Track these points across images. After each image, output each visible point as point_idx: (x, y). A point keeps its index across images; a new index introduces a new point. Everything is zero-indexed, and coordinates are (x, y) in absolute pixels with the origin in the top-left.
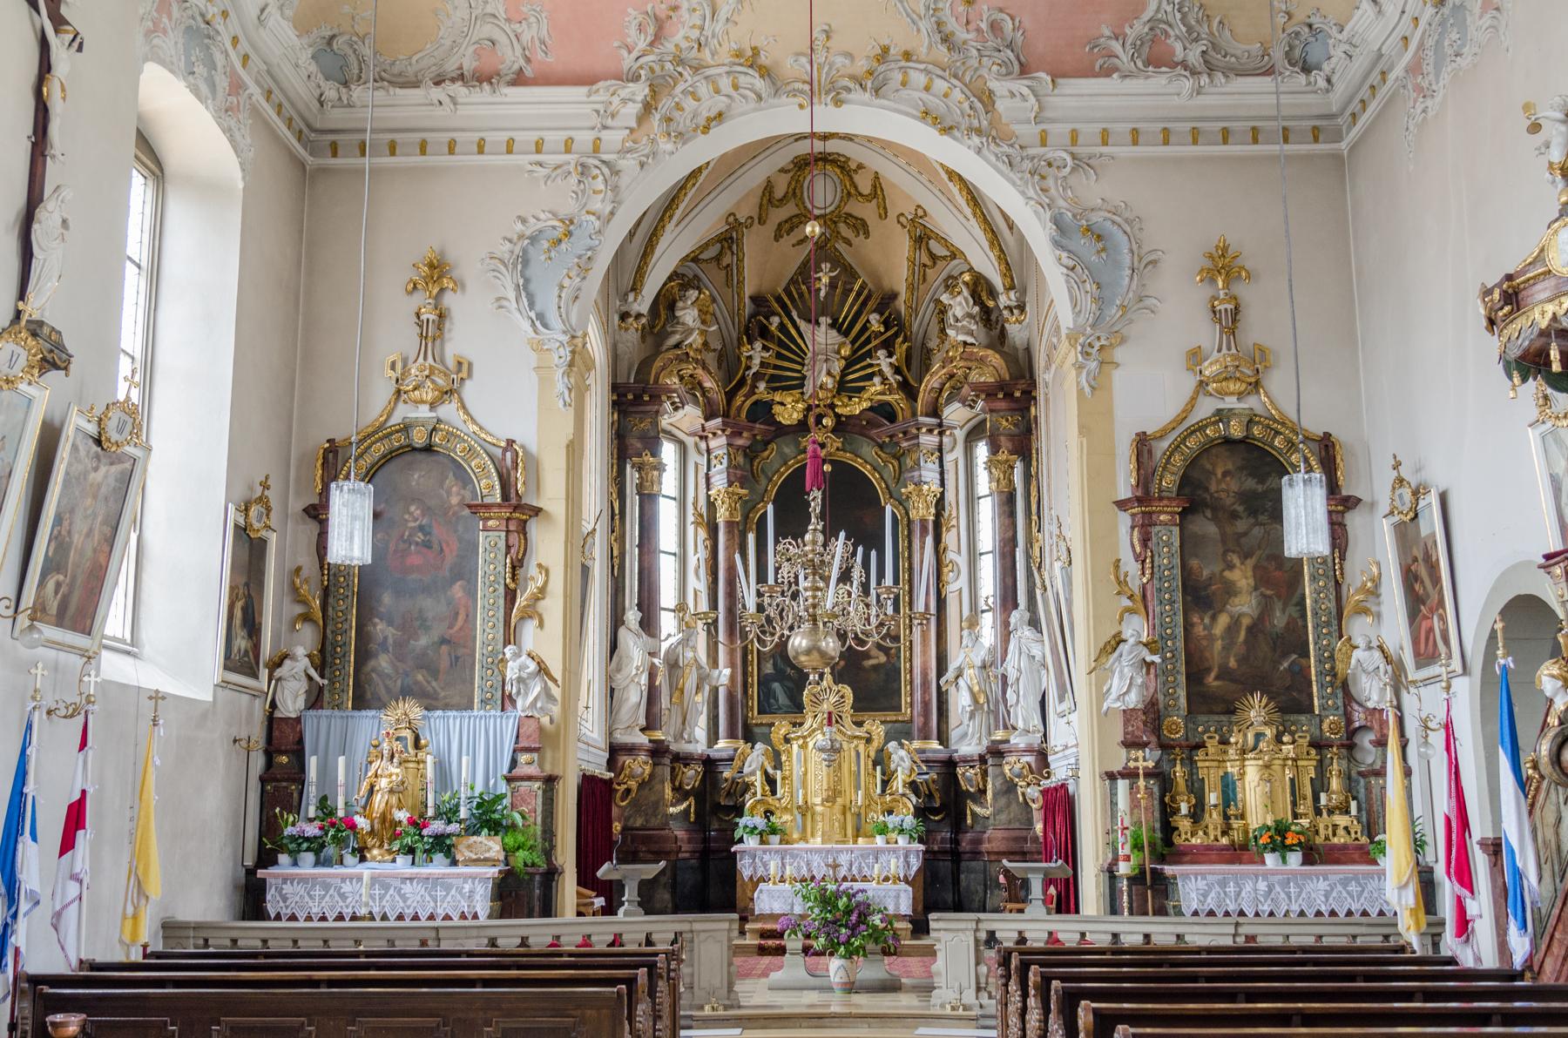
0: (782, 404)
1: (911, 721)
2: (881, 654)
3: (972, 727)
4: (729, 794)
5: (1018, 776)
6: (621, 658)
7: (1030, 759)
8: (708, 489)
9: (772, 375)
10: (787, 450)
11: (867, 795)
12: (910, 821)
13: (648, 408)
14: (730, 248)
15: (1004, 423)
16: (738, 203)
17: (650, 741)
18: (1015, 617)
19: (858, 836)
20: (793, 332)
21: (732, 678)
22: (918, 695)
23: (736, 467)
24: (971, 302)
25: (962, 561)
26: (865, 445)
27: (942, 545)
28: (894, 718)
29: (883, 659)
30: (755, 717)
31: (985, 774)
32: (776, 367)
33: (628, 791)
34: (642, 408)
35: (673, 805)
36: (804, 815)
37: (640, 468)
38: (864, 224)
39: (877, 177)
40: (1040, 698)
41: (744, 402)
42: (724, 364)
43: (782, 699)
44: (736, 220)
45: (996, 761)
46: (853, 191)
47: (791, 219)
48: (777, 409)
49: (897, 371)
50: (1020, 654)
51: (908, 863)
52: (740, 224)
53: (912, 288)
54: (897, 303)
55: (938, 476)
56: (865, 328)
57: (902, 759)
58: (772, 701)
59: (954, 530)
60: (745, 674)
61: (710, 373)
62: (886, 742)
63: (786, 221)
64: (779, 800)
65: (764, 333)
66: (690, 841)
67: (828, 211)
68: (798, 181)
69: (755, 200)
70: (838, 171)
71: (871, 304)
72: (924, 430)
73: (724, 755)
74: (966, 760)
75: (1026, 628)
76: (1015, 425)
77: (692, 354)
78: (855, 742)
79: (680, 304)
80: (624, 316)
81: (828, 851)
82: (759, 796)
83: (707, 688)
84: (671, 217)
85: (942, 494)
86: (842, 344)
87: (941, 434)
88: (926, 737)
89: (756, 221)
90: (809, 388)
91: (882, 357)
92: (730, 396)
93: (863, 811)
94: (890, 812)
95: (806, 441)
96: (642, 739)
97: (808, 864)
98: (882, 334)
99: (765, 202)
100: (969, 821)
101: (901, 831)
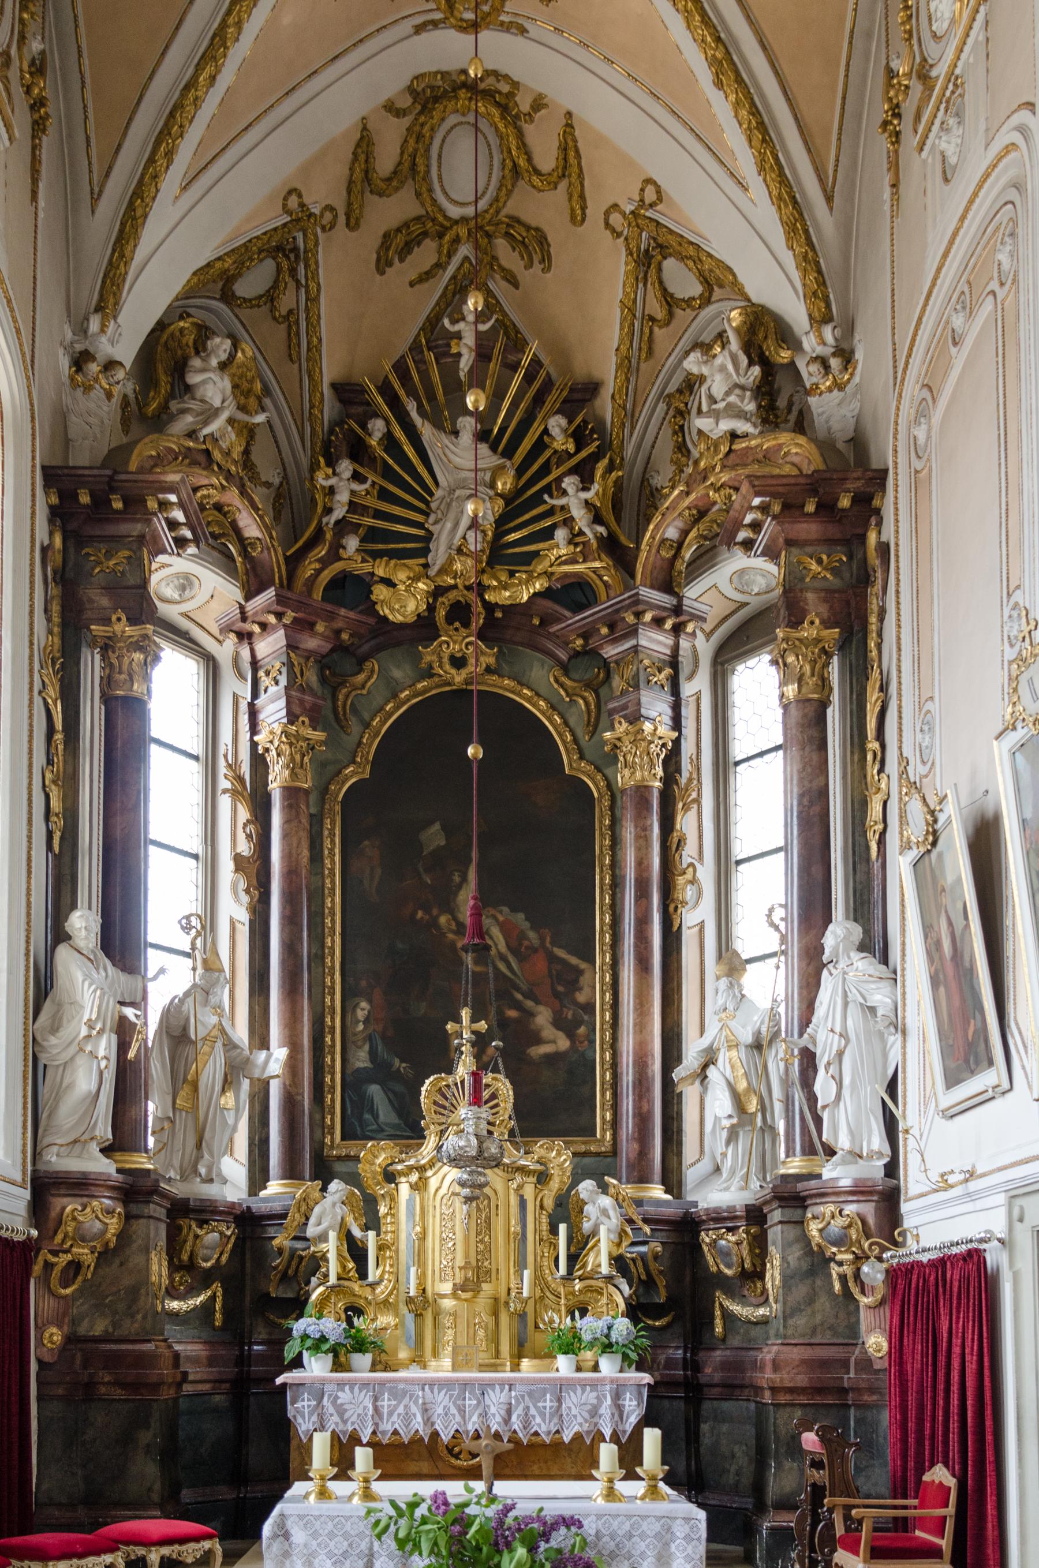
0: (389, 583)
1: (615, 1152)
2: (560, 1035)
3: (732, 1158)
4: (284, 1278)
5: (839, 1242)
6: (60, 1005)
7: (868, 1210)
8: (254, 729)
10: (397, 674)
11: (539, 1279)
12: (623, 1326)
13: (124, 528)
14: (293, 272)
15: (814, 566)
16: (306, 170)
17: (119, 1171)
21: (292, 1064)
22: (628, 1104)
23: (302, 689)
24: (744, 360)
25: (706, 874)
26: (536, 664)
29: (563, 1043)
30: (335, 1142)
31: (759, 1244)
32: (378, 514)
33: (76, 1266)
34: (111, 529)
35: (172, 1293)
36: (419, 1316)
37: (107, 647)
38: (542, 240)
39: (569, 114)
41: (318, 572)
42: (286, 514)
43: (385, 1113)
44: (302, 205)
45: (794, 1214)
46: (522, 162)
47: (406, 225)
48: (380, 592)
50: (846, 1004)
51: (619, 1409)
52: (311, 215)
53: (627, 366)
54: (598, 402)
55: (669, 712)
56: (540, 445)
57: (604, 1212)
58: (367, 1116)
59: (693, 813)
60: (319, 1069)
61: (256, 509)
62: (575, 1182)
63: (398, 230)
64: (373, 1286)
65: (358, 451)
66: (211, 1361)
67: (482, 204)
68: (419, 137)
69: (338, 170)
70: (495, 112)
71: (553, 399)
72: (648, 617)
73: (277, 1207)
74: (721, 1218)
75: (855, 956)
76: (834, 571)
77: (217, 455)
78: (519, 1178)
79: (196, 362)
80: (80, 360)
81: (465, 1385)
82: (333, 1280)
83: (246, 1084)
84: (170, 155)
85: (677, 742)
86: (497, 471)
87: (677, 630)
88: (643, 1178)
89: (342, 219)
90: (438, 555)
91: (571, 490)
92: (293, 562)
93: (530, 1309)
95: (428, 655)
96: (105, 1167)
97: (425, 1411)
98: (571, 456)
99: (358, 175)
100: (719, 1329)
101: (608, 1347)
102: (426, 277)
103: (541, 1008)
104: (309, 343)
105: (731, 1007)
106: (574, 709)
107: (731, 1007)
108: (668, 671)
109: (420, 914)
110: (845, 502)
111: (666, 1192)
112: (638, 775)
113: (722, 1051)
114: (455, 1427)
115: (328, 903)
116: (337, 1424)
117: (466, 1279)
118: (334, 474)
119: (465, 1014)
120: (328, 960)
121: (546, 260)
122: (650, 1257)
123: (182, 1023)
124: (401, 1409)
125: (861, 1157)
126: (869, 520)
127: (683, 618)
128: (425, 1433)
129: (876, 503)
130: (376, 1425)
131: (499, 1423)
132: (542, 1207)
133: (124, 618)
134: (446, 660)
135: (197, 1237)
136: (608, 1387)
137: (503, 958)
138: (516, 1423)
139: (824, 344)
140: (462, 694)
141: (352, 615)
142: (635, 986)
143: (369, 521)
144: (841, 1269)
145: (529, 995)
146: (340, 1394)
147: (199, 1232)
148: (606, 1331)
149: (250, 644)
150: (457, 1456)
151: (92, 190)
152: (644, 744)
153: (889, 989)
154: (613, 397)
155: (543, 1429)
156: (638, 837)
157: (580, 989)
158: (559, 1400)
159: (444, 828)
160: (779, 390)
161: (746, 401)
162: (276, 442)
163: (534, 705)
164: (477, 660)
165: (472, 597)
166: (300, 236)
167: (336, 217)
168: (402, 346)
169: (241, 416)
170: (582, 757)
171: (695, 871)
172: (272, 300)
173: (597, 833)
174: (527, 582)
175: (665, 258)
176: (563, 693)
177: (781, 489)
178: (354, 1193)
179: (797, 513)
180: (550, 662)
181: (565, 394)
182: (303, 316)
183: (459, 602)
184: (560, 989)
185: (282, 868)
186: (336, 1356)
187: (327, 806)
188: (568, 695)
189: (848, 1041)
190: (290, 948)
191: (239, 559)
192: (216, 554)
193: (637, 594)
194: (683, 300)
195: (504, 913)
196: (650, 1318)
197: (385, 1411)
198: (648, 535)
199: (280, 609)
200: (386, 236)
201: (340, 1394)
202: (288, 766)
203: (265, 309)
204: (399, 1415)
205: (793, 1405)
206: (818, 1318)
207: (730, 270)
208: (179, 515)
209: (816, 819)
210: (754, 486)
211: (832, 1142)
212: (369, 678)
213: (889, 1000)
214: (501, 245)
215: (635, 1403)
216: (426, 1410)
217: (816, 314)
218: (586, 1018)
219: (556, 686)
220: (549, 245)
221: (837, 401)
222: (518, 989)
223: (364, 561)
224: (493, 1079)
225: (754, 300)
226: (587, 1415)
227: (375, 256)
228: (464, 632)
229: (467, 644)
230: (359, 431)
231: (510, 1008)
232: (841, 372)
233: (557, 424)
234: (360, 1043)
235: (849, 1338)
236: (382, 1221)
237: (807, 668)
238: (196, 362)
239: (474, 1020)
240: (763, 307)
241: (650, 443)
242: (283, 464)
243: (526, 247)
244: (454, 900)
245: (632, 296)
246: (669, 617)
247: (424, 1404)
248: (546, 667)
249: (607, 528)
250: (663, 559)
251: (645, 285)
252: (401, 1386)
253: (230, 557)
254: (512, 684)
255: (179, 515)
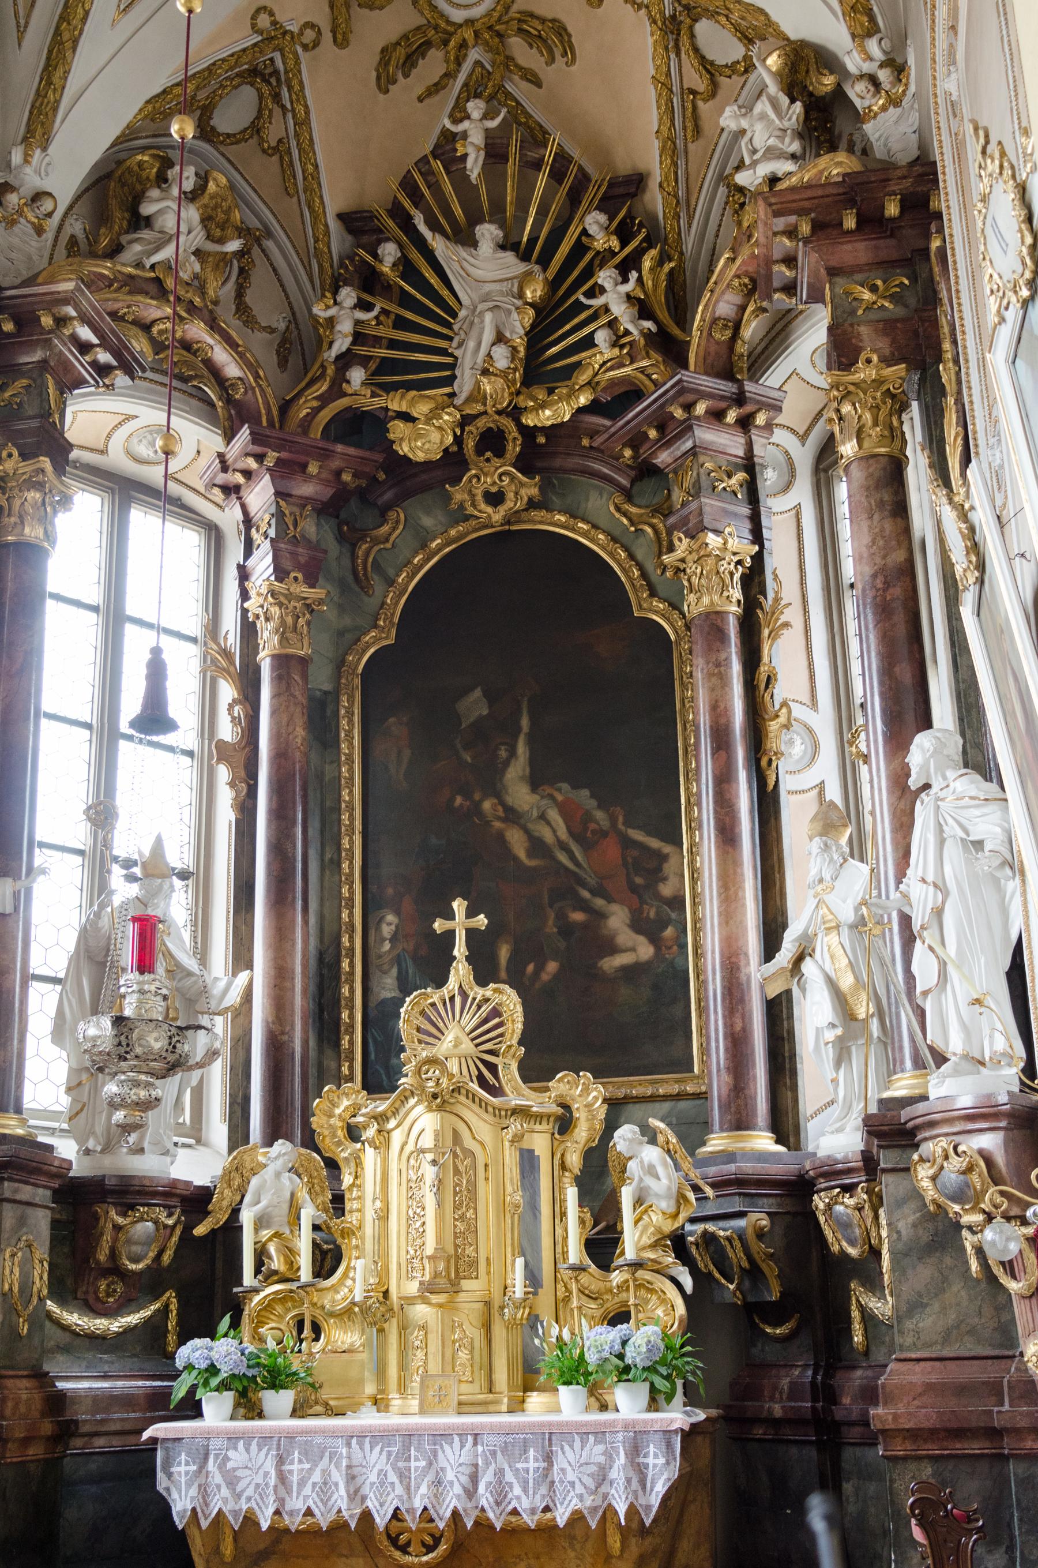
0: (407, 417)
2: (641, 939)
5: (958, 1197)
8: (245, 595)
9: (384, 359)
10: (427, 521)
14: (277, 97)
15: (867, 295)
18: (922, 747)
19: (528, 1387)
20: (434, 280)
24: (785, 100)
26: (594, 495)
27: (763, 670)
28: (676, 1089)
29: (645, 951)
32: (393, 344)
38: (561, 30)
40: (1006, 963)
41: (316, 411)
44: (274, 23)
47: (405, 37)
48: (398, 429)
49: (643, 309)
50: (941, 842)
51: (639, 1472)
53: (671, 149)
54: (647, 197)
56: (580, 248)
63: (398, 43)
72: (701, 408)
76: (893, 298)
77: (170, 283)
78: (515, 1125)
85: (758, 559)
86: (524, 279)
87: (745, 423)
88: (741, 1123)
89: (327, 36)
90: (465, 382)
91: (608, 285)
94: (620, 1318)
95: (458, 494)
97: (351, 1478)
98: (614, 254)
100: (858, 1338)
102: (436, 88)
103: (615, 908)
104: (303, 172)
105: (827, 877)
106: (641, 540)
107: (827, 877)
108: (741, 476)
109: (459, 800)
110: (892, 209)
111: (777, 1142)
112: (706, 600)
113: (820, 936)
114: (396, 1503)
115: (345, 795)
116: (225, 1500)
117: (436, 1275)
118: (336, 303)
119: (459, 906)
120: (345, 866)
121: (569, 50)
122: (750, 1235)
123: (103, 943)
124: (316, 1477)
125: (982, 1063)
126: (929, 229)
127: (748, 408)
128: (351, 1516)
129: (933, 205)
130: (282, 1501)
131: (458, 1497)
132: (563, 1167)
133: (16, 453)
134: (479, 498)
135: (117, 1228)
136: (620, 1437)
137: (563, 847)
138: (485, 1497)
139: (871, 59)
140: (503, 538)
141: (352, 451)
142: (718, 865)
143: (384, 352)
144: (975, 1238)
145: (599, 891)
146: (231, 1454)
147: (120, 1220)
148: (617, 1347)
149: (239, 498)
150: (404, 1549)
151: (18, 22)
152: (711, 561)
153: (999, 813)
154: (661, 185)
155: (524, 1505)
156: (710, 675)
157: (665, 879)
158: (549, 1459)
159: (486, 694)
160: (840, 136)
161: (787, 140)
162: (282, 285)
163: (592, 540)
164: (516, 493)
165: (508, 425)
166: (277, 56)
167: (319, 33)
168: (409, 162)
169: (211, 247)
170: (653, 594)
171: (790, 712)
172: (258, 132)
173: (677, 683)
174: (569, 396)
175: (696, 21)
176: (625, 521)
177: (806, 204)
178: (310, 1160)
179: (835, 232)
180: (610, 488)
181: (603, 189)
182: (293, 143)
183: (490, 429)
184: (639, 880)
185: (270, 751)
186: (243, 1394)
187: (343, 681)
188: (632, 524)
189: (946, 893)
190: (279, 850)
191: (219, 404)
192: (194, 402)
193: (680, 381)
194: (726, 66)
195: (564, 791)
196: (770, 1324)
197: (295, 1479)
198: (698, 317)
199: (258, 449)
200: (384, 50)
201: (231, 1454)
202: (277, 631)
203: (253, 141)
204: (314, 1484)
205: (919, 1458)
206: (952, 1317)
207: (762, 11)
208: (85, 333)
209: (897, 605)
210: (770, 205)
211: (939, 1045)
212: (394, 529)
213: (998, 830)
214: (517, 45)
215: (662, 1461)
216: (353, 1477)
217: (859, 31)
218: (673, 916)
219: (617, 515)
220: (569, 36)
221: (894, 118)
222: (583, 884)
223: (374, 395)
224: (495, 990)
225: (793, 36)
226: (590, 1483)
227: (374, 74)
228: (496, 462)
229: (500, 476)
230: (369, 258)
231: (575, 909)
232: (893, 85)
233: (595, 222)
234: (386, 967)
235: (1001, 1346)
236: (347, 1196)
237: (868, 417)
238: (155, 193)
239: (471, 913)
240: (802, 41)
241: (714, 233)
242: (292, 308)
243: (544, 41)
244: (501, 780)
245: (664, 69)
246: (729, 407)
247: (349, 1467)
248: (605, 496)
249: (656, 322)
250: (718, 343)
251: (678, 54)
252: (318, 1440)
253: (212, 405)
254: (563, 519)
255: (85, 333)
